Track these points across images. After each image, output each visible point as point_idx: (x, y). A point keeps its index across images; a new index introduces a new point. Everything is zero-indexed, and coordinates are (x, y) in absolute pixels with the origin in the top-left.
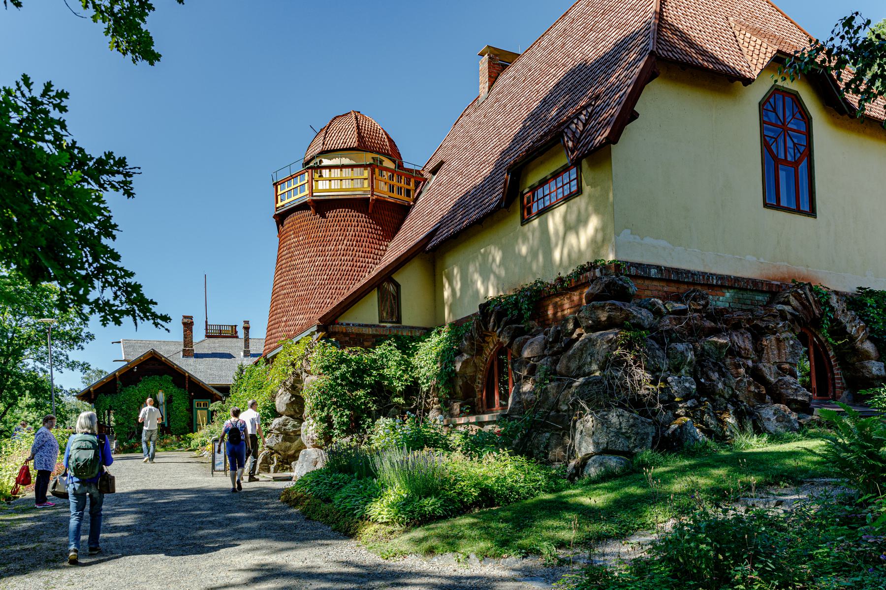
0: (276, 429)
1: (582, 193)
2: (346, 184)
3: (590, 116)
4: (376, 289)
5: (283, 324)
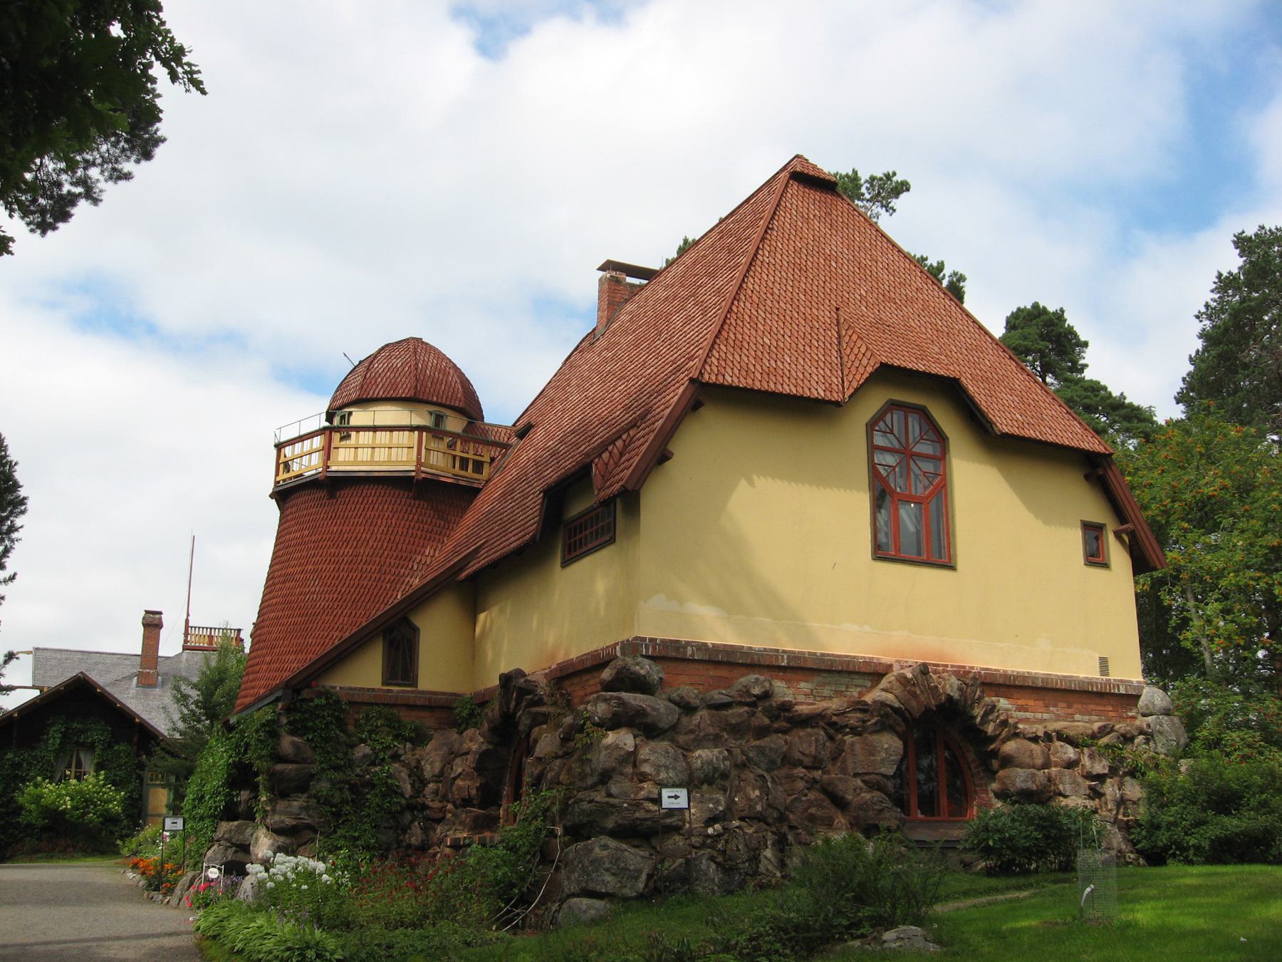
0: (226, 840)
1: (615, 541)
2: (381, 455)
3: (625, 447)
4: (381, 638)
5: (265, 667)
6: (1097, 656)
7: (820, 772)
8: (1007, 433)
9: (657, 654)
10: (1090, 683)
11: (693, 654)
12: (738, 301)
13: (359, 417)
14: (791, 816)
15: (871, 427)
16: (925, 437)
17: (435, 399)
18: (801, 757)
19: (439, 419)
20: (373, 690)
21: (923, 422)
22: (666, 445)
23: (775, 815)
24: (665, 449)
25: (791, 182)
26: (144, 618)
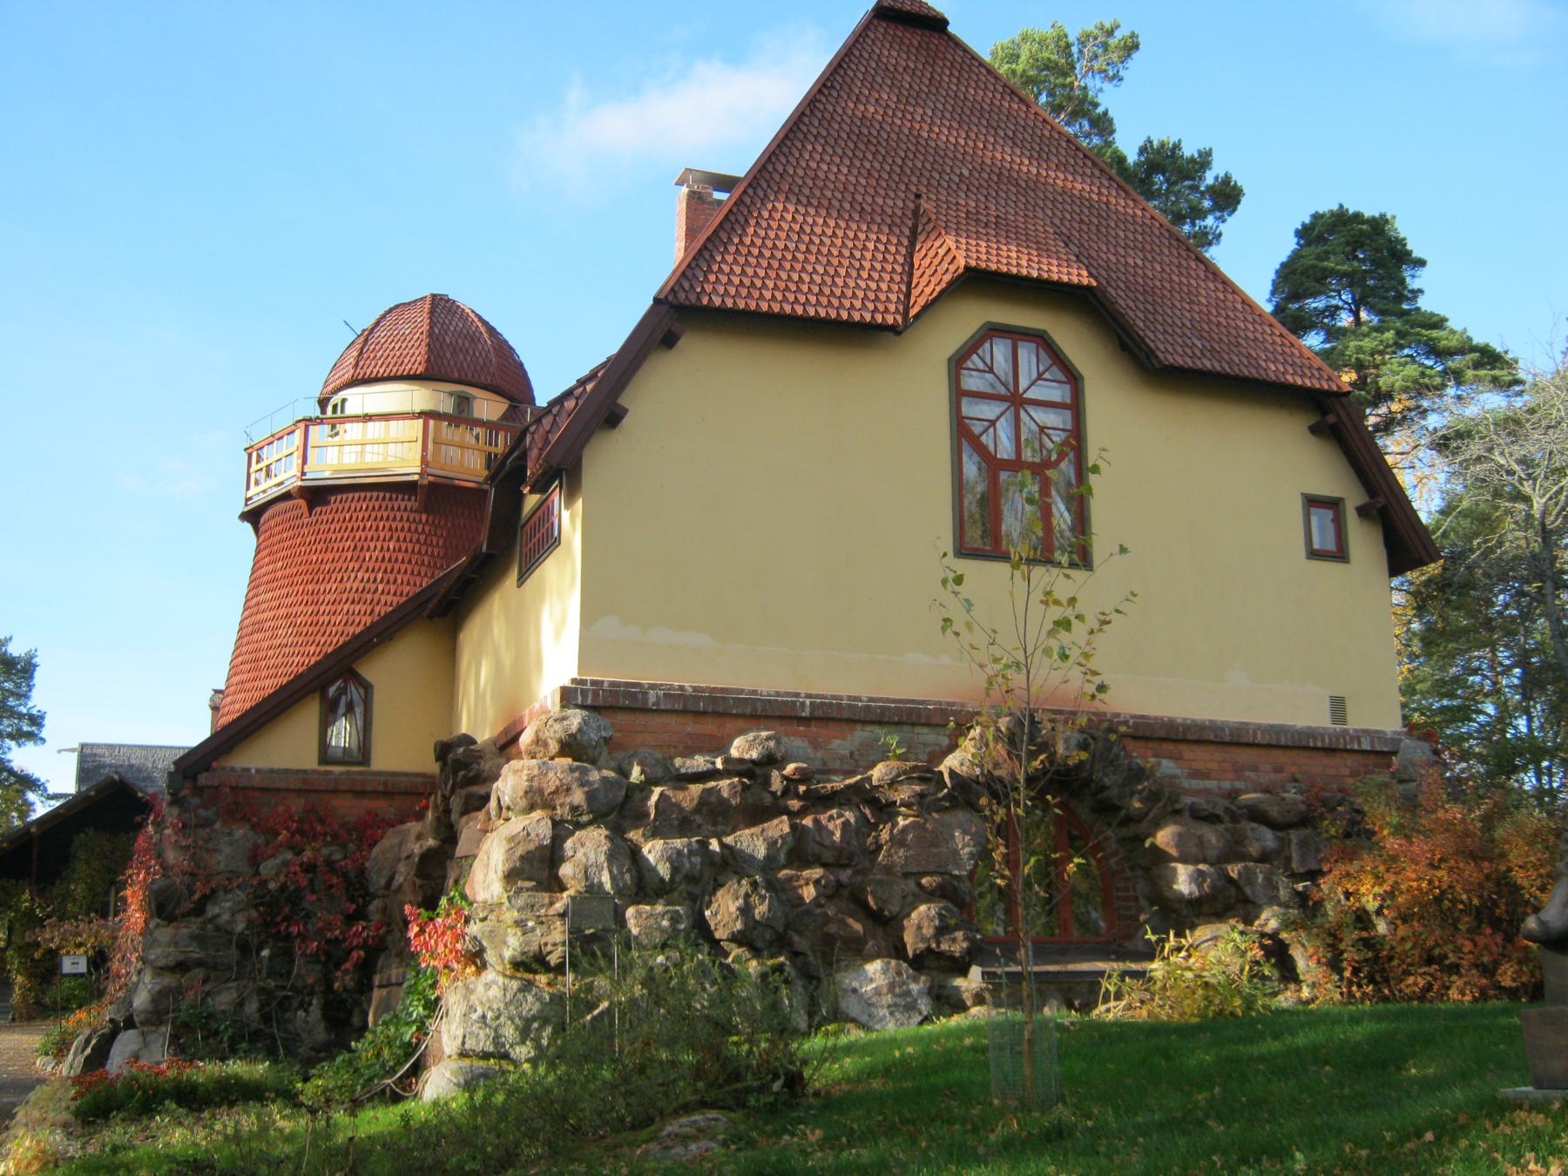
6: (1326, 694)
7: (849, 872)
8: (1172, 366)
9: (600, 702)
10: (1312, 733)
11: (657, 703)
12: (755, 189)
13: (359, 400)
14: (796, 938)
15: (958, 363)
16: (1046, 376)
17: (456, 375)
18: (817, 849)
19: (463, 402)
20: (305, 771)
21: (1043, 354)
22: (618, 395)
23: (768, 936)
24: (614, 403)
25: (876, 22)
26: (211, 700)
